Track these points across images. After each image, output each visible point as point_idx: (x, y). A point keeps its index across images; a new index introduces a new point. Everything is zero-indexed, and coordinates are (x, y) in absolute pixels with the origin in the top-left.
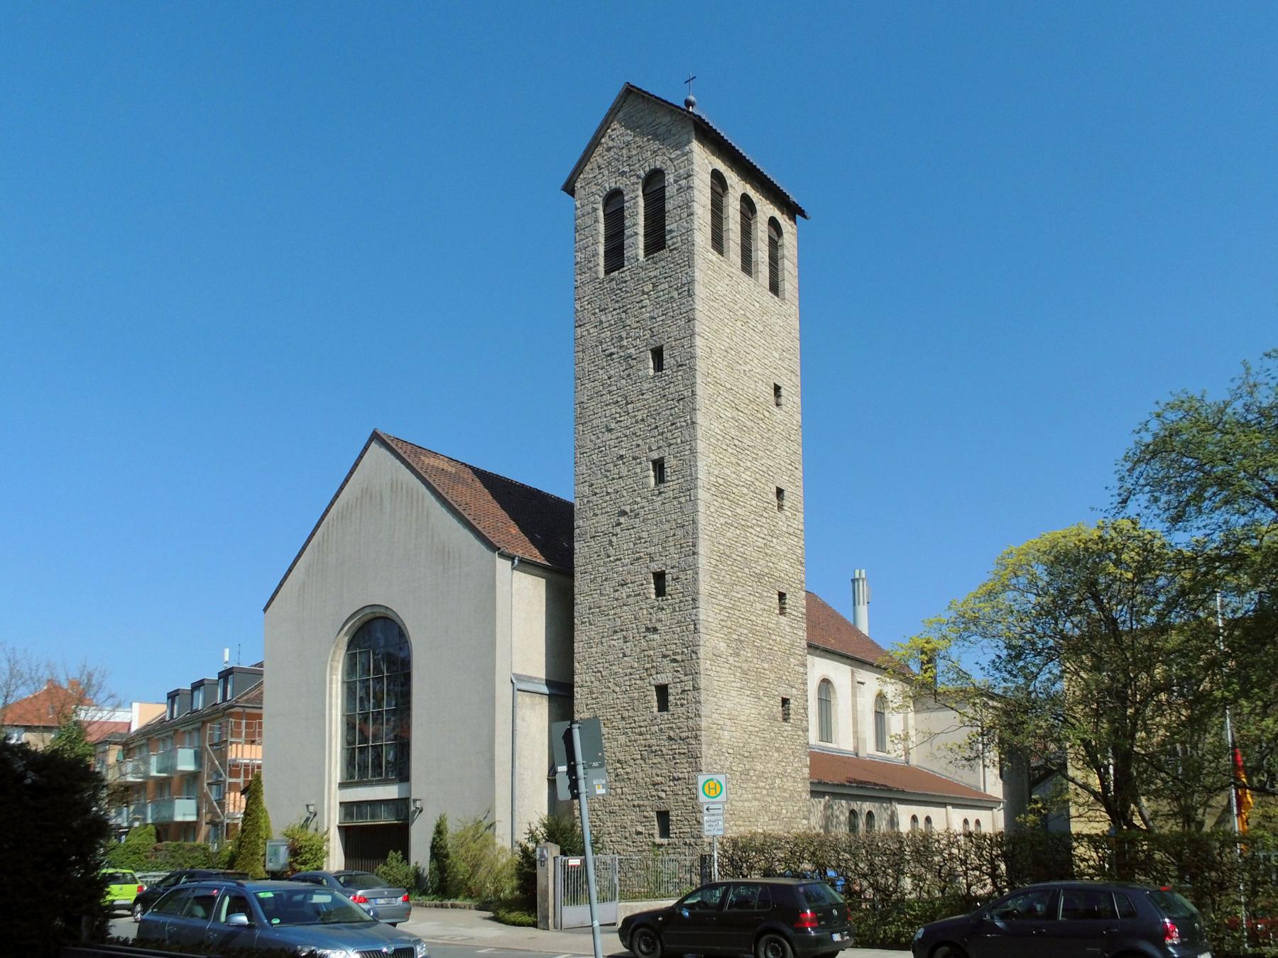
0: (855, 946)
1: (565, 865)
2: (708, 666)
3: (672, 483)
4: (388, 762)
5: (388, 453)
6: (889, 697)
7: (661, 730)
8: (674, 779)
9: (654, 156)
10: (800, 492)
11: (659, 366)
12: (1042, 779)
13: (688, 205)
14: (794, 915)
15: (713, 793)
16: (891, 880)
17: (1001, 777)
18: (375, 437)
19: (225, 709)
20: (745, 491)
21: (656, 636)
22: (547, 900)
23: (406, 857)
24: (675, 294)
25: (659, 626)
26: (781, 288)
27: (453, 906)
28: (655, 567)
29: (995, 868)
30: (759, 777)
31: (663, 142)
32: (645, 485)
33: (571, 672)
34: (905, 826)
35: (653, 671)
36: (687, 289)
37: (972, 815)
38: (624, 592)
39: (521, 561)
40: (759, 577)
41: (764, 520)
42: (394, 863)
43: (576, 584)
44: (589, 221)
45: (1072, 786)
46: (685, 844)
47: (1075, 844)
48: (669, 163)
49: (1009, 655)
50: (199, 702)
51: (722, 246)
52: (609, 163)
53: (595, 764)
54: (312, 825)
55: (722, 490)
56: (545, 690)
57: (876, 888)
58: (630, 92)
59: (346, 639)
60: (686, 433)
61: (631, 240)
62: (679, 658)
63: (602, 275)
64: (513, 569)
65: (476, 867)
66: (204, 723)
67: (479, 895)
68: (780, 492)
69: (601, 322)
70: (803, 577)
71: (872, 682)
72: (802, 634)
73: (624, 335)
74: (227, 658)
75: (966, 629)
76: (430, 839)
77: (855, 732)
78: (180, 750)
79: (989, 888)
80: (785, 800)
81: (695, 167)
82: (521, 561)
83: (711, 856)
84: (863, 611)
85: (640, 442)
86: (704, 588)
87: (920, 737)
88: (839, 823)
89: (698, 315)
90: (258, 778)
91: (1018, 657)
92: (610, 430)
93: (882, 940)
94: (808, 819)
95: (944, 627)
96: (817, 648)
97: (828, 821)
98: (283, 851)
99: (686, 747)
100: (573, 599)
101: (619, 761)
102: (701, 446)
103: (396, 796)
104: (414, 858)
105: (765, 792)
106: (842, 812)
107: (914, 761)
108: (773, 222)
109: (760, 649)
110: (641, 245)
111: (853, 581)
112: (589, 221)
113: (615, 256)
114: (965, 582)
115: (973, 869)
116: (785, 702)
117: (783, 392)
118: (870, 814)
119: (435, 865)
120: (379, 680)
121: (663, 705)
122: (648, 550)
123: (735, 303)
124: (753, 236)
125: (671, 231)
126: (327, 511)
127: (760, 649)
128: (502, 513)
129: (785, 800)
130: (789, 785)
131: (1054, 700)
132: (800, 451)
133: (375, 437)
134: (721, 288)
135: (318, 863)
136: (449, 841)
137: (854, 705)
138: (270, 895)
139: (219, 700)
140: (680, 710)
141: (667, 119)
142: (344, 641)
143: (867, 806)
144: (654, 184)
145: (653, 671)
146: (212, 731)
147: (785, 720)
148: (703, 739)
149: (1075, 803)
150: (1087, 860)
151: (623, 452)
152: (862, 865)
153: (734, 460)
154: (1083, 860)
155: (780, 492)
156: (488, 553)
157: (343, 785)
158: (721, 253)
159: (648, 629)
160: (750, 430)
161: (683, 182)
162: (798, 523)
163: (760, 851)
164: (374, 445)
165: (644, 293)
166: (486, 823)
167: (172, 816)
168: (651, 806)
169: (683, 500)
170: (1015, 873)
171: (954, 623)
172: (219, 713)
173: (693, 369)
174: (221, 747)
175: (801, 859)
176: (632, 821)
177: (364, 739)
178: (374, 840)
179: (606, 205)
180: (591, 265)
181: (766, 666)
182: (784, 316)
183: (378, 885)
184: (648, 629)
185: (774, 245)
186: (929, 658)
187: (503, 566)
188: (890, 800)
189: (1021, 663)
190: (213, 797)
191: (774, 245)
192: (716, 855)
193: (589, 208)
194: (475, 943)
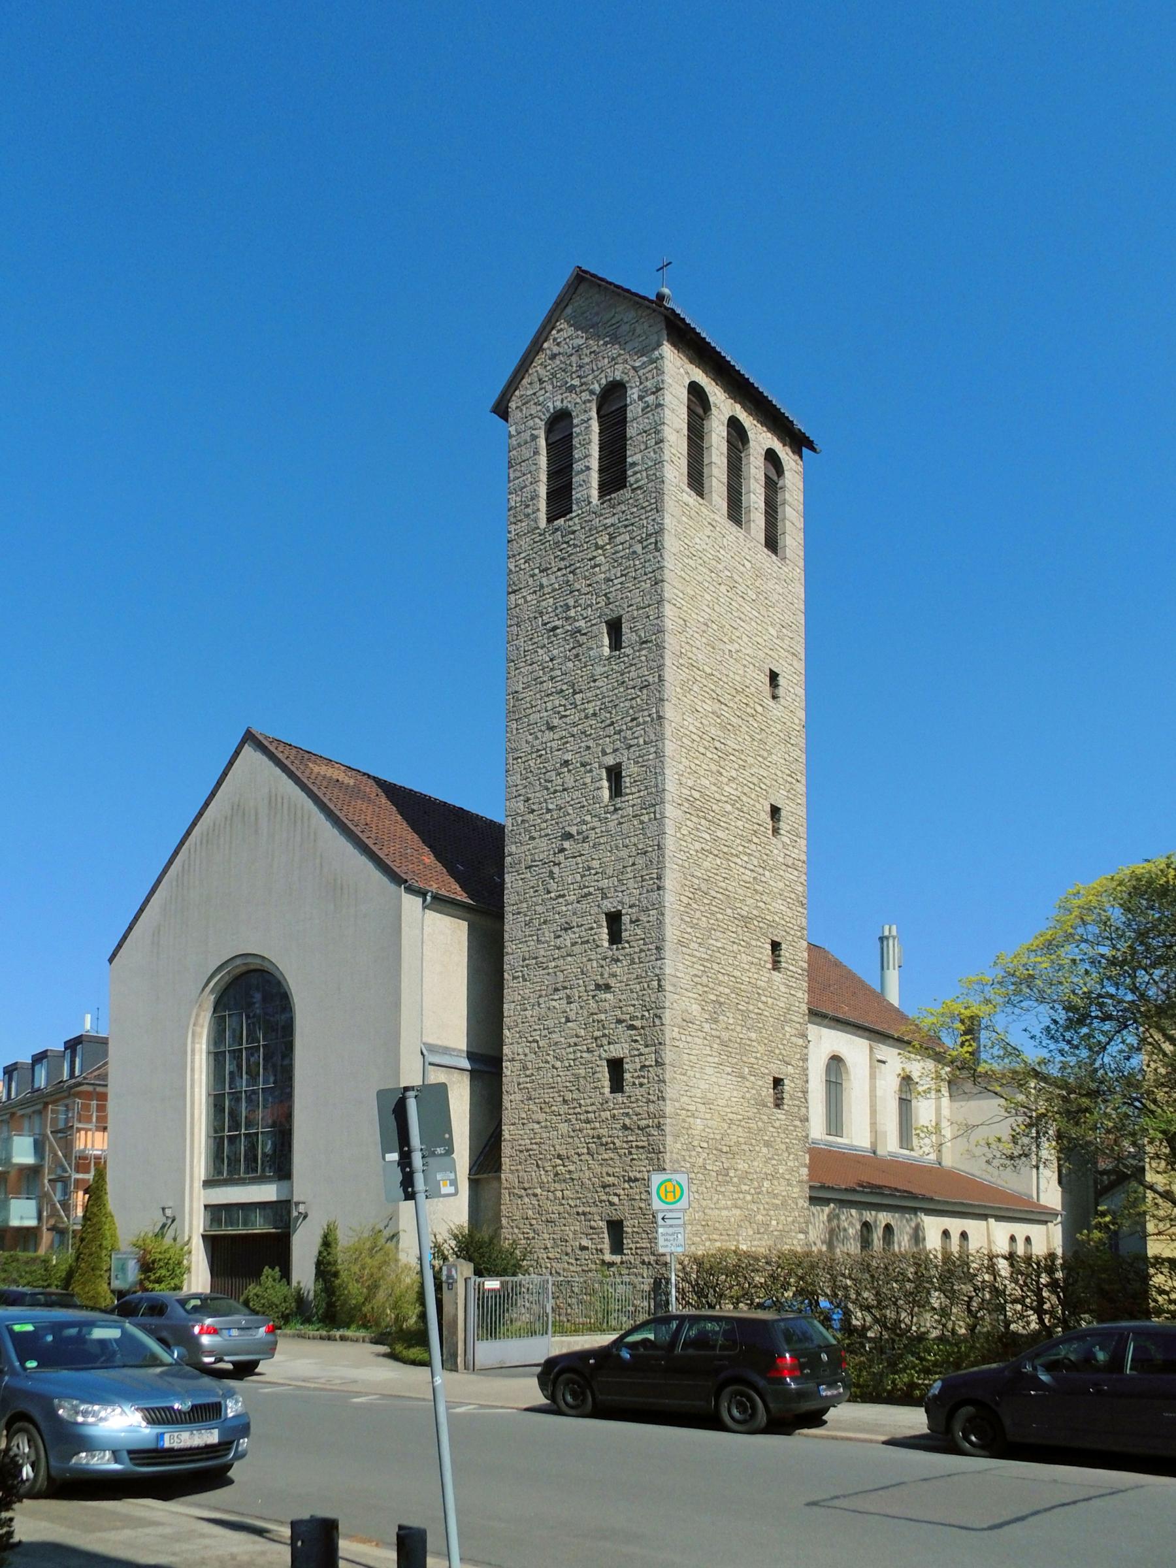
0: (853, 1399)
1: (480, 1287)
2: (675, 1035)
3: (632, 797)
4: (264, 1154)
5: (265, 759)
6: (915, 1076)
7: (614, 1116)
8: (630, 1180)
9: (614, 364)
10: (802, 811)
11: (616, 643)
12: (1112, 1186)
13: (656, 430)
14: (768, 1361)
15: (670, 1198)
16: (903, 1315)
17: (1060, 1183)
18: (249, 737)
19: (70, 1088)
20: (729, 808)
21: (609, 996)
22: (455, 1333)
23: (286, 1274)
24: (638, 548)
25: (612, 982)
26: (780, 544)
27: (343, 1338)
28: (609, 905)
29: (1041, 1301)
30: (741, 1178)
31: (623, 346)
32: (597, 800)
33: (499, 1042)
34: (933, 1242)
35: (605, 1041)
36: (654, 541)
37: (1021, 1230)
38: (568, 938)
39: (435, 897)
40: (746, 920)
41: (753, 847)
42: (270, 1283)
43: (506, 927)
44: (526, 452)
45: (1150, 1194)
46: (643, 1263)
47: (1152, 1271)
48: (632, 373)
49: (1068, 1019)
50: (41, 1080)
51: (702, 485)
52: (554, 375)
53: (440, 1150)
54: (170, 1234)
55: (697, 807)
56: (466, 1065)
57: (881, 1322)
58: (581, 278)
59: (212, 997)
60: (650, 731)
61: (582, 477)
62: (638, 1023)
63: (543, 523)
64: (424, 908)
65: (374, 1287)
66: (46, 1104)
67: (377, 1324)
68: (775, 812)
69: (542, 586)
70: (804, 923)
71: (894, 1060)
72: (803, 996)
73: (571, 602)
74: (88, 1025)
75: (1018, 992)
76: (316, 1253)
77: (873, 1124)
78: (15, 1138)
79: (1034, 1326)
80: (776, 1207)
81: (666, 378)
82: (435, 897)
83: (668, 1281)
84: (893, 977)
85: (591, 743)
86: (671, 933)
87: (953, 1131)
88: (846, 1238)
89: (668, 575)
90: (101, 1175)
91: (1081, 1022)
92: (551, 728)
93: (889, 1392)
94: (806, 1233)
95: (987, 988)
96: (824, 1016)
97: (833, 1235)
98: (132, 1268)
99: (647, 1142)
100: (502, 947)
101: (559, 1157)
102: (670, 748)
103: (274, 1198)
104: (296, 1277)
105: (749, 1198)
106: (851, 1224)
107: (948, 1162)
108: (771, 457)
109: (745, 1014)
110: (595, 483)
111: (882, 939)
112: (526, 452)
113: (561, 499)
114: (1017, 939)
115: (1014, 1302)
116: (777, 1082)
117: (781, 681)
118: (888, 1228)
119: (320, 1286)
120: (252, 1051)
121: (617, 1085)
122: (600, 884)
123: (719, 561)
124: (744, 474)
125: (634, 464)
126: (188, 833)
127: (745, 1014)
128: (413, 838)
129: (776, 1207)
130: (781, 1188)
131: (1130, 1082)
132: (803, 759)
133: (249, 737)
134: (701, 540)
135: (176, 1281)
136: (341, 1254)
137: (873, 1089)
138: (29, 1328)
139: (65, 1077)
140: (638, 1091)
141: (630, 315)
142: (209, 1000)
143: (884, 1218)
144: (612, 401)
145: (605, 1041)
146: (55, 1114)
147: (777, 1106)
148: (668, 1129)
149: (1153, 1216)
150: (1167, 1293)
151: (568, 757)
152: (866, 1294)
153: (714, 768)
154: (1161, 1292)
155: (775, 812)
156: (393, 887)
157: (208, 1184)
158: (700, 494)
159: (598, 987)
160: (736, 729)
161: (650, 399)
162: (799, 851)
163: (732, 1272)
164: (248, 750)
165: (597, 547)
166: (387, 1233)
167: (7, 1220)
168: (600, 1214)
169: (645, 818)
170: (1072, 1305)
171: (1000, 983)
172: (63, 1093)
173: (660, 647)
174: (65, 1135)
175: (785, 1286)
176: (575, 1232)
177: (235, 1125)
178: (248, 1253)
179: (549, 431)
180: (529, 510)
181: (753, 1036)
182: (787, 580)
183: (236, 1312)
184: (598, 987)
185: (772, 487)
186: (972, 1029)
187: (411, 904)
188: (915, 1210)
189: (1085, 1030)
190: (57, 1198)
191: (772, 487)
192: (673, 1278)
193: (526, 436)
194: (355, 1388)
